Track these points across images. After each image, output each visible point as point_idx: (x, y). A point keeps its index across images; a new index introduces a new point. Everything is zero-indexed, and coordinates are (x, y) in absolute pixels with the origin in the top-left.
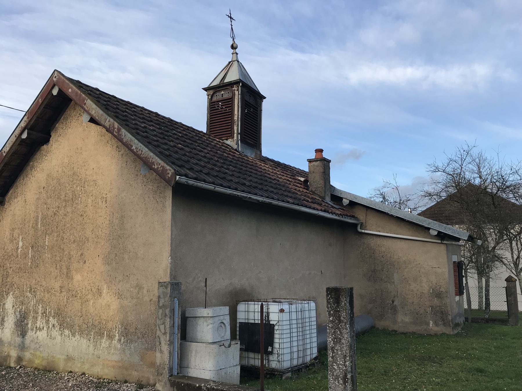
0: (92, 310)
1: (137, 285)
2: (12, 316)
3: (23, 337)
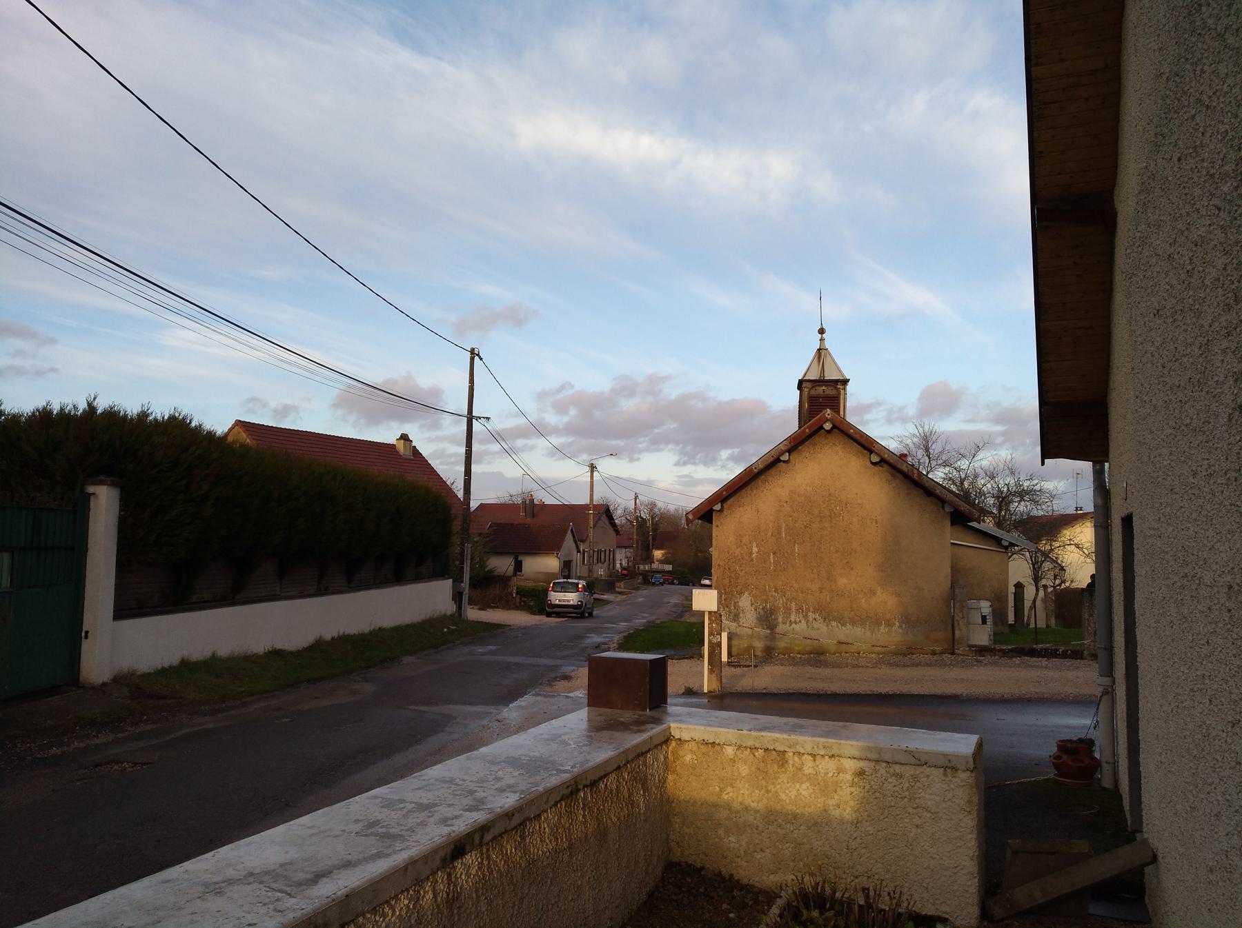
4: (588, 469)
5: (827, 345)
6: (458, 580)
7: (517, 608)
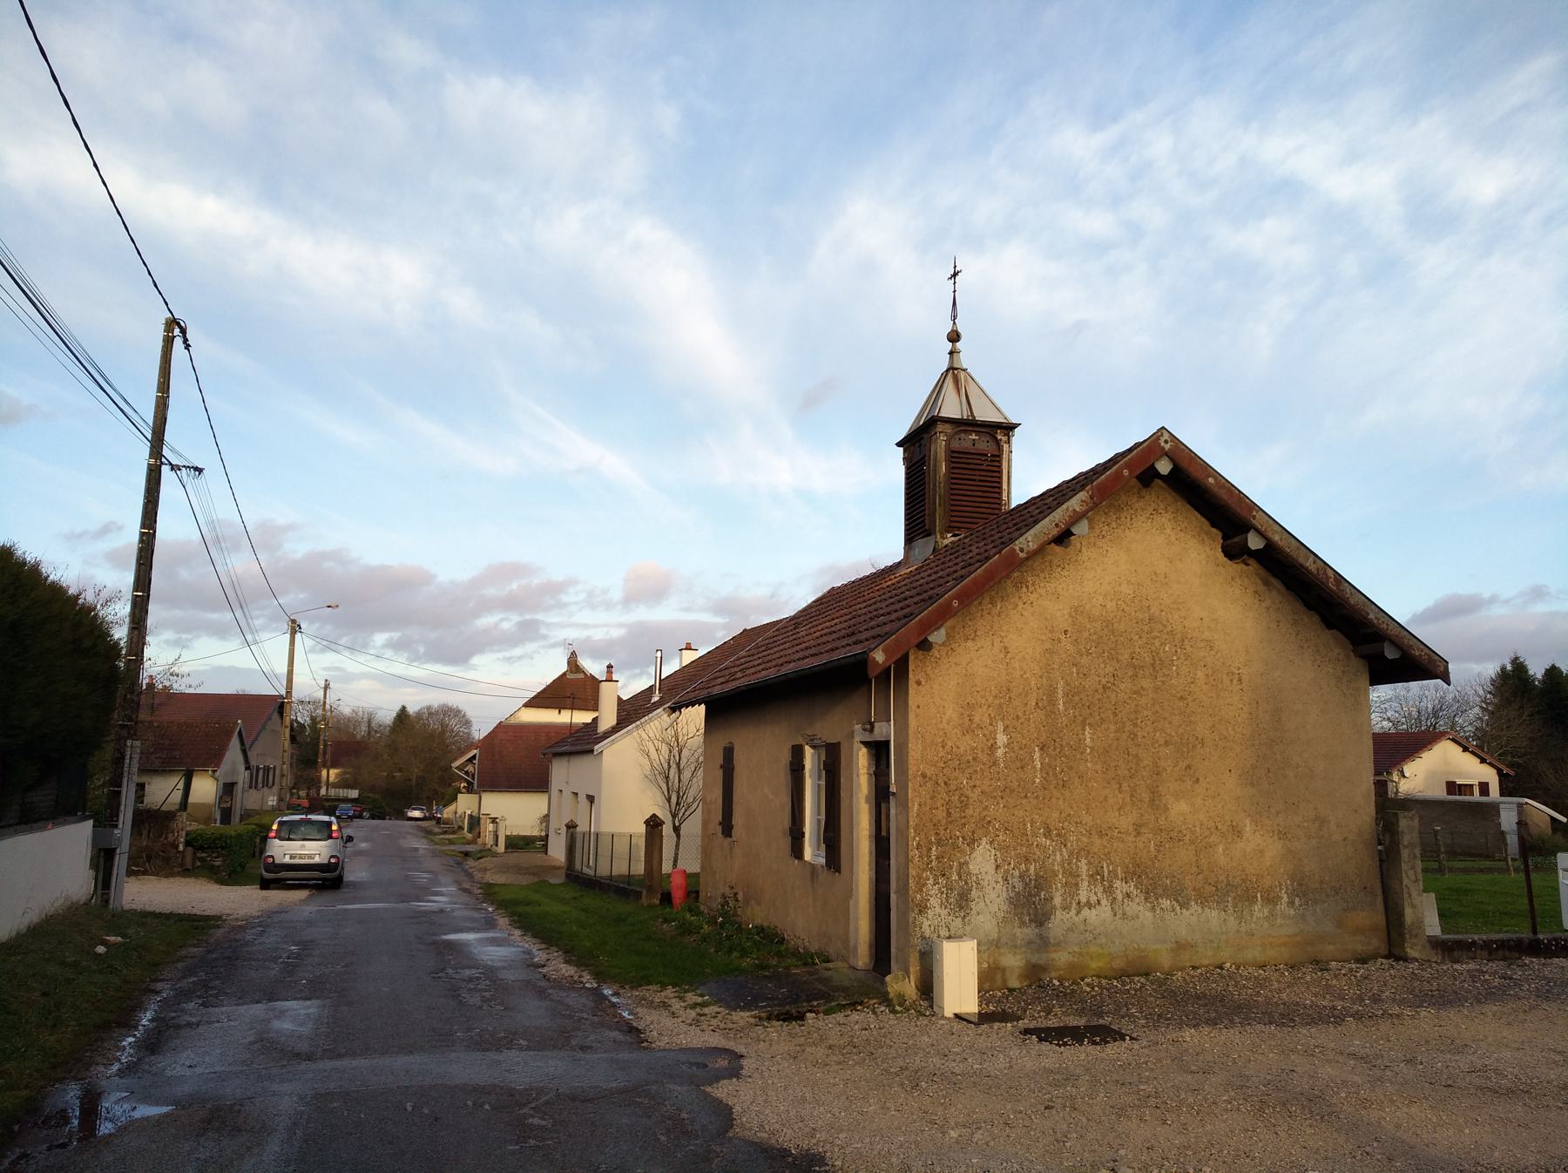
0: (1223, 861)
1: (1317, 818)
2: (999, 886)
3: (1040, 924)
4: (285, 627)
5: (965, 360)
6: (105, 819)
7: (187, 872)
